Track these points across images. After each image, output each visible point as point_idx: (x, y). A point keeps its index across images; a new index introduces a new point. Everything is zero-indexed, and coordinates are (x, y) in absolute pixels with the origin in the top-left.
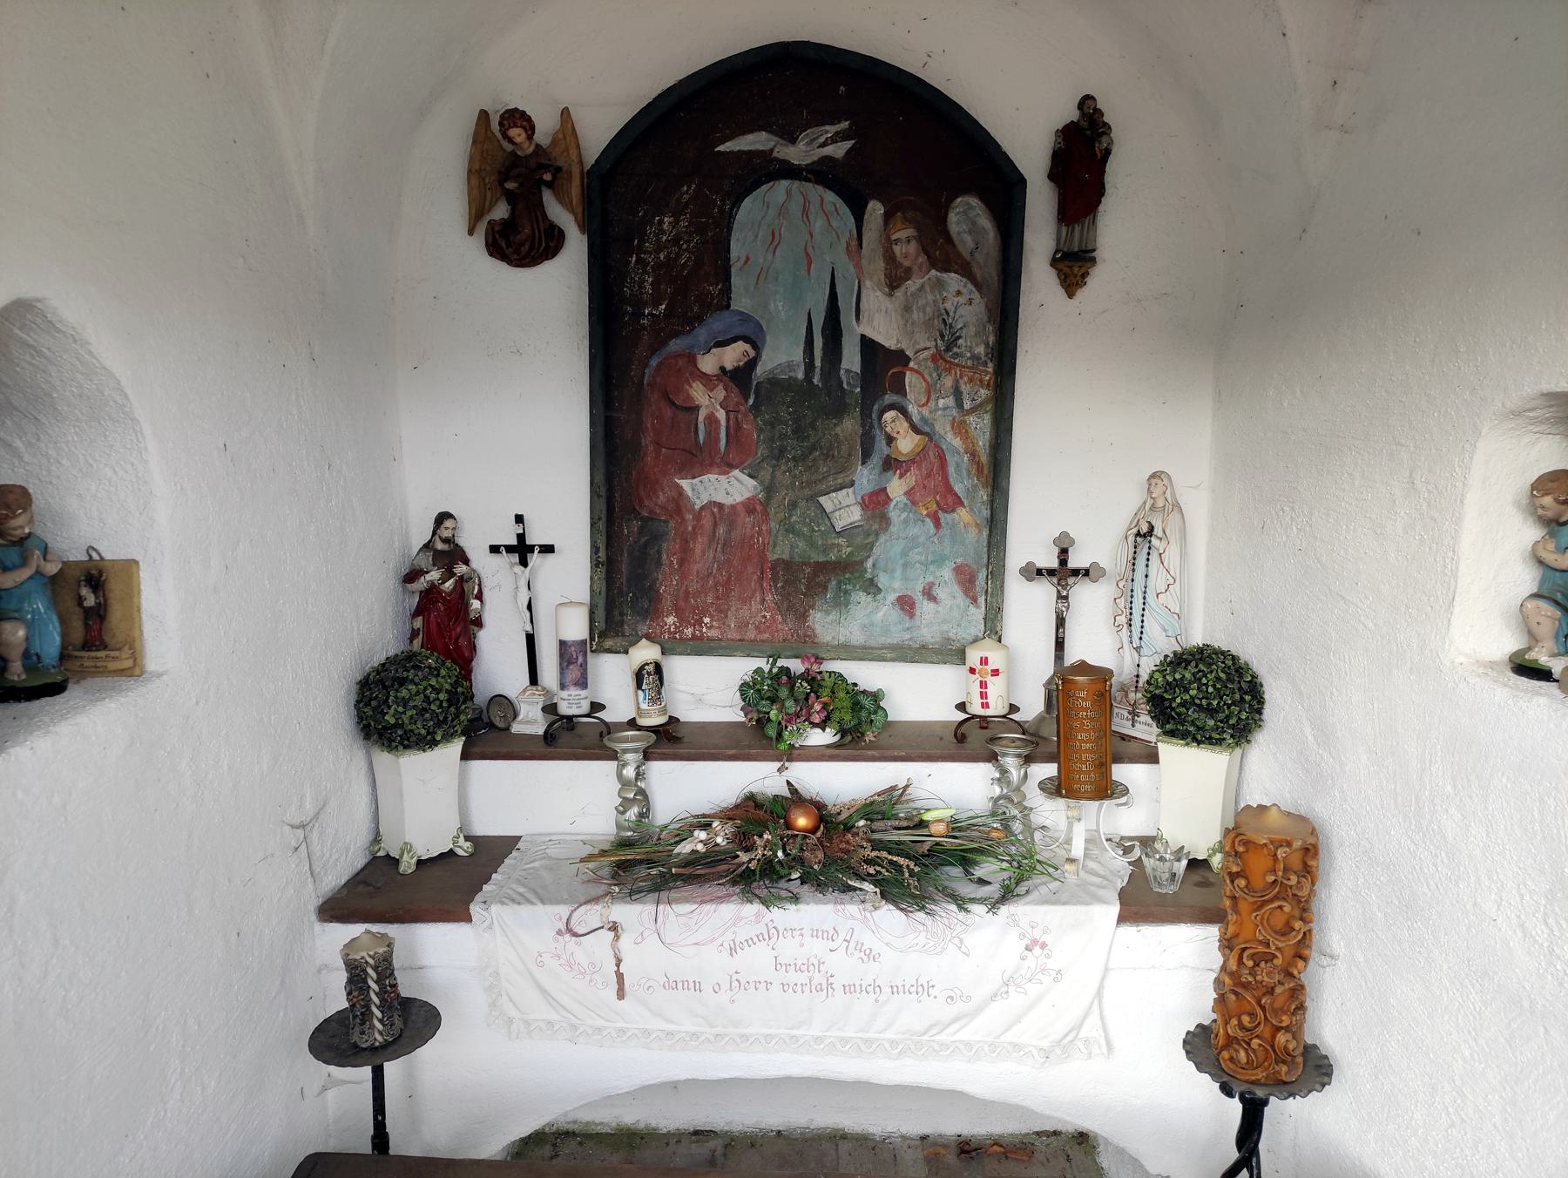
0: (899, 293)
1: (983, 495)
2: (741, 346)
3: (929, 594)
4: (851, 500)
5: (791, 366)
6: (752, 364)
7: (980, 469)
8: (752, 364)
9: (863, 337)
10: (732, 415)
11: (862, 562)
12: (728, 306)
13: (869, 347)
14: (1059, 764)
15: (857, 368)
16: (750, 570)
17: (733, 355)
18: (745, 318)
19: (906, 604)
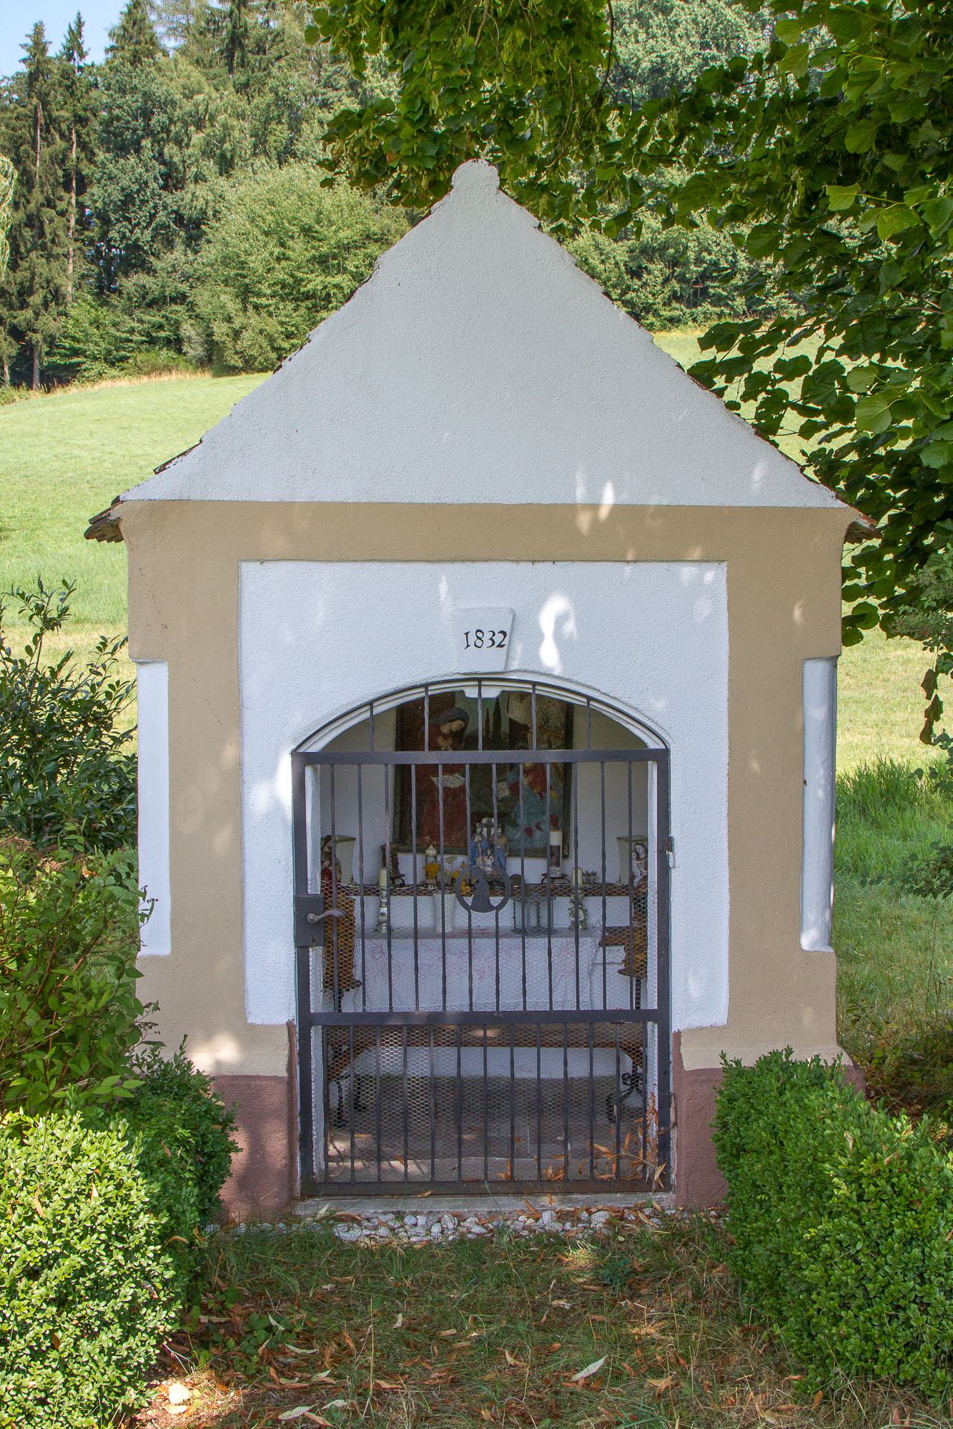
0: (524, 701)
1: (561, 785)
2: (459, 722)
3: (538, 827)
4: (505, 787)
5: (518, 1004)
6: (463, 729)
7: (559, 774)
8: (463, 729)
9: (510, 719)
10: (652, 1002)
11: (509, 813)
12: (453, 706)
13: (513, 723)
14: (722, 1029)
15: (507, 731)
16: (916, 242)
17: (456, 725)
18: (461, 711)
19: (529, 832)
